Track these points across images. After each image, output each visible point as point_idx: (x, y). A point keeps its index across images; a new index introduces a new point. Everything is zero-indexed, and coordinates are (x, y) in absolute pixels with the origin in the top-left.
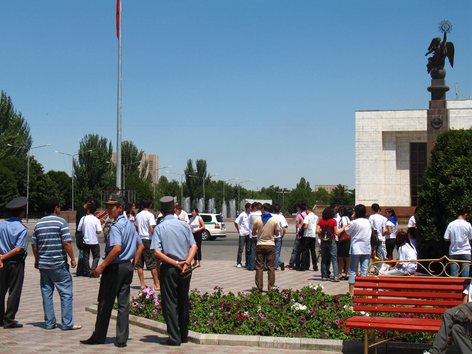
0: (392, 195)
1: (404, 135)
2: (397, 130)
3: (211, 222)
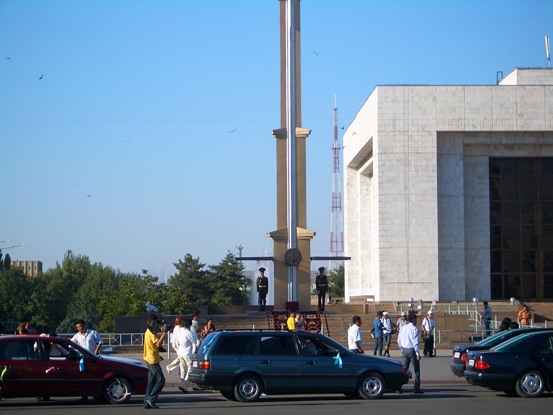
0: (457, 271)
1: (481, 140)
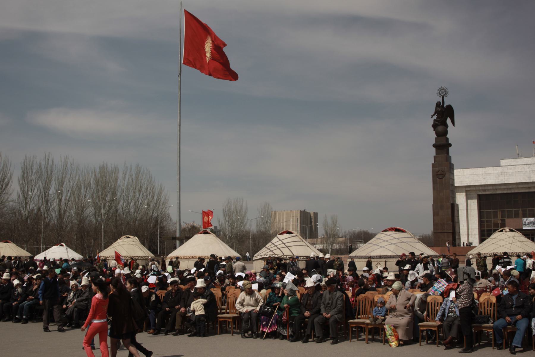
2: (466, 185)
3: (397, 260)
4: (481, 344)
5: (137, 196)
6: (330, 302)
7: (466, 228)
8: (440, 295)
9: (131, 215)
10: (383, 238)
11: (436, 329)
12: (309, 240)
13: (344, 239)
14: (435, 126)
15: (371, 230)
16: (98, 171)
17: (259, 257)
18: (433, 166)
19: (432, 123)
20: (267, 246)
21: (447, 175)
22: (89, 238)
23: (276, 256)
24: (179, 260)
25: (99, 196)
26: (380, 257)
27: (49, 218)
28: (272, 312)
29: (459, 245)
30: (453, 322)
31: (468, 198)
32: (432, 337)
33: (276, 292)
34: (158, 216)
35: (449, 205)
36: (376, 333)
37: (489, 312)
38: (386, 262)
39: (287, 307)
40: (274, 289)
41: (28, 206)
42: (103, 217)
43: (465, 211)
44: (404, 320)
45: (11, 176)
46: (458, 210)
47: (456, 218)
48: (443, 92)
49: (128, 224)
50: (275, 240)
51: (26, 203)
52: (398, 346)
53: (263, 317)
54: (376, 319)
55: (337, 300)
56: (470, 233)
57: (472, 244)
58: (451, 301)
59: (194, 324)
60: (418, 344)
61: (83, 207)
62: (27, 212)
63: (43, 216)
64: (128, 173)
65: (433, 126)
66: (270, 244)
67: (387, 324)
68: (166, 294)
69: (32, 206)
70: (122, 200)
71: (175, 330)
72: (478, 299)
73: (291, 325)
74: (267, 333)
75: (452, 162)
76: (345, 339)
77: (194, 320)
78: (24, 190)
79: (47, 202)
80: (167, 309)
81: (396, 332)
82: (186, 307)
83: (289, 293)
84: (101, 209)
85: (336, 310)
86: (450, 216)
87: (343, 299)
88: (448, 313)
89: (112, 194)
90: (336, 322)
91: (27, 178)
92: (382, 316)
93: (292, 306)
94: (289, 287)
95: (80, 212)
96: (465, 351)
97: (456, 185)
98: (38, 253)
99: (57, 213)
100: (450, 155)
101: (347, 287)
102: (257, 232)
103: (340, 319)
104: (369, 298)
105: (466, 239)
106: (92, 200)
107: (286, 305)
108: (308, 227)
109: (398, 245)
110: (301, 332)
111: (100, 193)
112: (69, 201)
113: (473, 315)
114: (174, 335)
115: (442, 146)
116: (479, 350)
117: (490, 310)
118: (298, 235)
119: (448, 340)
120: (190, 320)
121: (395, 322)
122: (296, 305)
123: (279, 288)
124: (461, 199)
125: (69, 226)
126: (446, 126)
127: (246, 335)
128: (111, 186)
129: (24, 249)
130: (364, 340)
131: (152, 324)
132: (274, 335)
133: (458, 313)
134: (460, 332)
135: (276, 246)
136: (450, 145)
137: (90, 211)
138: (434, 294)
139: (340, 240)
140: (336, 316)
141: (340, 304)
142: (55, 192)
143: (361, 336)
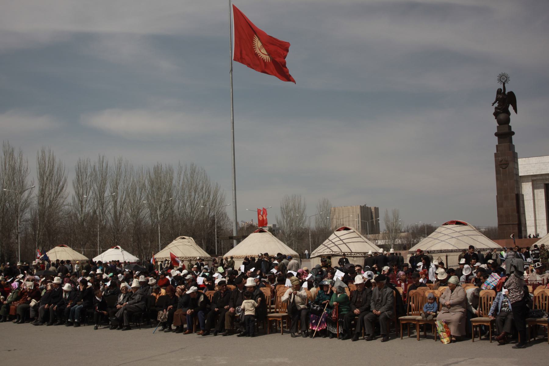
4: (536, 338)
5: (193, 196)
6: (380, 298)
7: (533, 219)
8: (493, 289)
9: (187, 216)
10: (443, 232)
11: (489, 324)
12: (370, 236)
13: (406, 233)
14: (496, 114)
15: (434, 224)
16: (152, 171)
17: (316, 255)
18: (496, 155)
19: (494, 111)
20: (324, 243)
21: (511, 165)
22: (144, 240)
23: (333, 253)
24: (234, 259)
25: (154, 198)
26: (441, 251)
27: (105, 221)
28: (322, 311)
29: (526, 237)
30: (506, 316)
31: (534, 188)
32: (486, 333)
33: (325, 289)
34: (214, 216)
35: (514, 195)
36: (428, 330)
37: (544, 305)
38: (447, 256)
39: (336, 305)
40: (322, 287)
41: (84, 210)
42: (159, 218)
43: (532, 201)
44: (455, 315)
45: (65, 180)
46: (523, 201)
47: (521, 209)
48: (504, 79)
49: (185, 224)
50: (332, 237)
51: (82, 207)
52: (450, 342)
53: (312, 315)
54: (427, 315)
55: (387, 296)
56: (538, 224)
57: (538, 235)
58: (504, 295)
59: (243, 324)
60: (471, 340)
61: (139, 209)
62: (83, 215)
63: (99, 219)
64: (183, 173)
65: (494, 114)
66: (327, 240)
67: (439, 320)
68: (214, 294)
69: (88, 209)
70: (178, 201)
71: (225, 330)
72: (533, 293)
73: (341, 323)
74: (317, 332)
75: (516, 151)
76: (397, 336)
77: (243, 319)
78: (79, 193)
79: (102, 204)
80: (216, 309)
81: (448, 328)
82: (234, 307)
83: (338, 290)
84: (156, 211)
85: (386, 306)
86: (515, 207)
87: (393, 295)
88: (502, 308)
89: (168, 195)
90: (386, 318)
91: (82, 181)
92: (433, 312)
93: (341, 303)
94: (337, 285)
95: (136, 215)
96: (519, 347)
97: (520, 175)
98: (95, 255)
99: (112, 216)
100: (513, 143)
101: (399, 282)
102: (317, 229)
103: (390, 316)
104: (419, 294)
105: (534, 230)
106: (148, 201)
107: (335, 303)
108: (369, 223)
109: (459, 238)
110: (351, 332)
111: (155, 194)
112: (124, 203)
113: (528, 309)
114: (224, 335)
115: (505, 135)
116: (534, 346)
117: (545, 304)
118: (355, 231)
119: (501, 335)
120: (240, 320)
121: (447, 318)
122: (346, 302)
123: (327, 286)
124: (527, 189)
125: (125, 228)
126: (509, 114)
127: (296, 334)
128: (166, 187)
129: (81, 253)
130: (415, 337)
131: (201, 325)
132: (324, 333)
133: (510, 307)
134: (513, 327)
135: (333, 243)
136: (513, 133)
137: (145, 213)
138: (486, 288)
139: (403, 234)
140: (386, 313)
141: (390, 300)
142: (110, 194)
143: (413, 333)
